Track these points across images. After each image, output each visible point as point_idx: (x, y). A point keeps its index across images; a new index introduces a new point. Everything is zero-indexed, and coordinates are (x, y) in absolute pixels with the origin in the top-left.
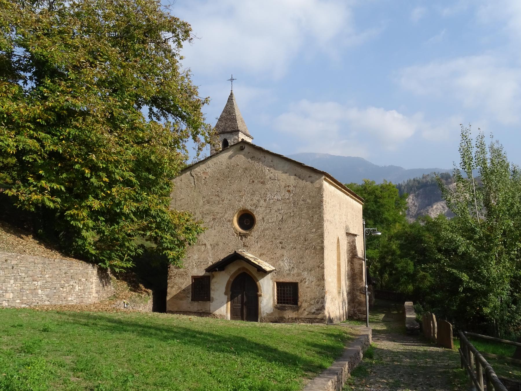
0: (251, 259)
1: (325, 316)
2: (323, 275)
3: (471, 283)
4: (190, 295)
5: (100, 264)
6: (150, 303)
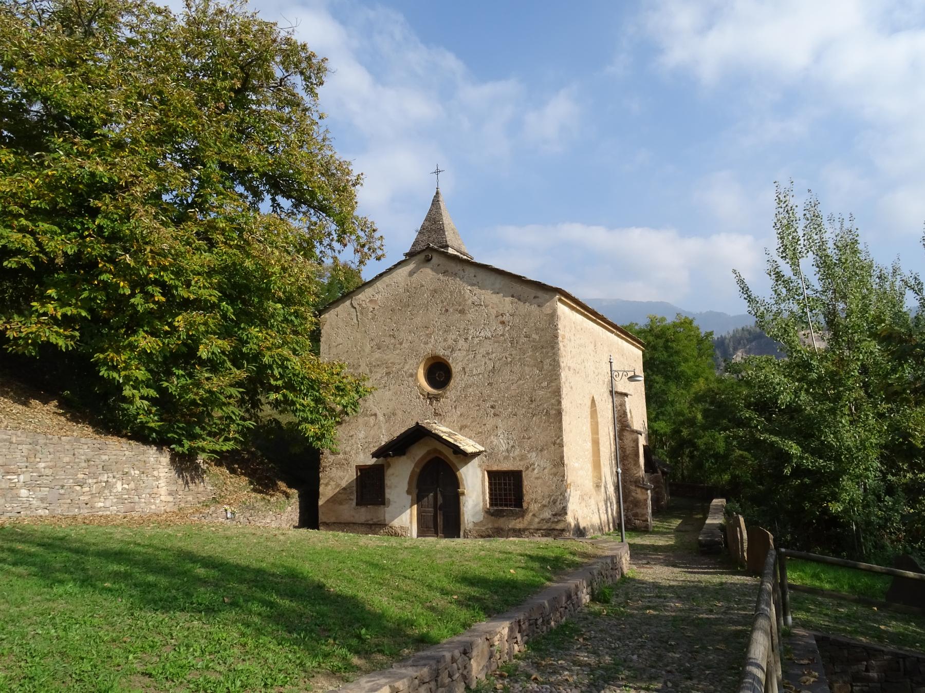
0: (442, 435)
1: (570, 524)
2: (562, 458)
3: (807, 459)
4: (354, 497)
5: (172, 446)
6: (292, 510)
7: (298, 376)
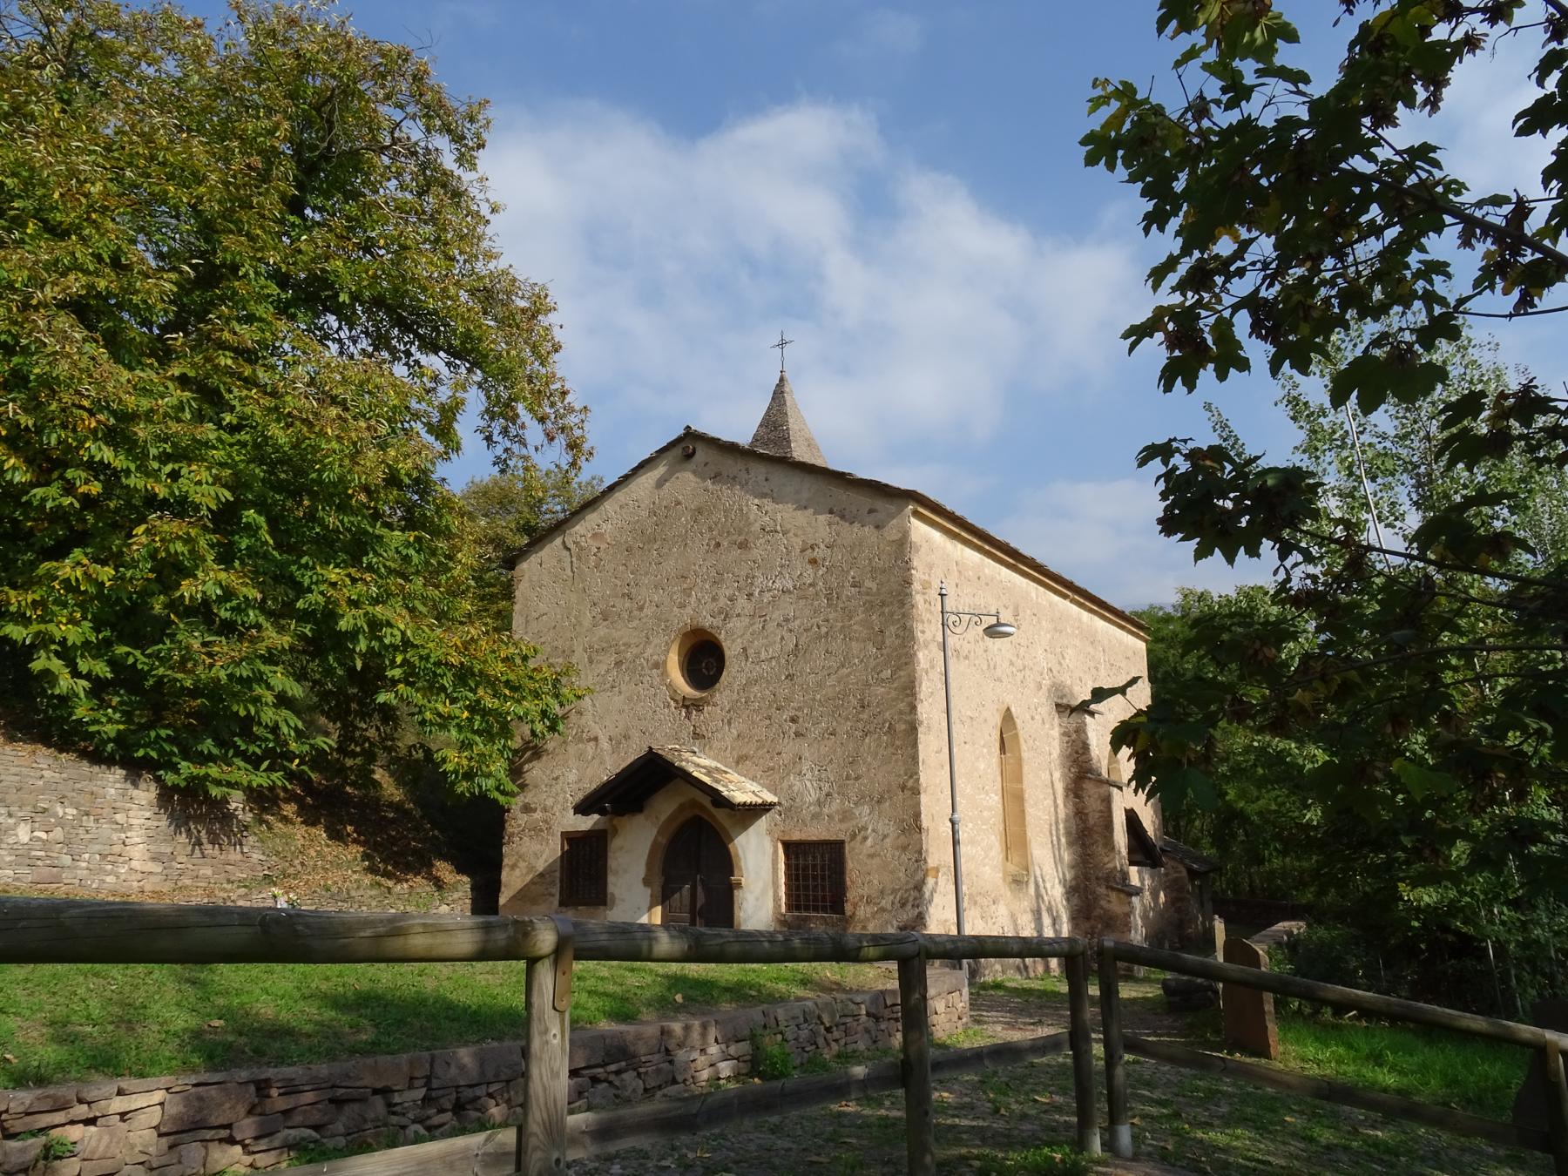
2: (917, 816)
4: (556, 890)
7: (427, 658)
